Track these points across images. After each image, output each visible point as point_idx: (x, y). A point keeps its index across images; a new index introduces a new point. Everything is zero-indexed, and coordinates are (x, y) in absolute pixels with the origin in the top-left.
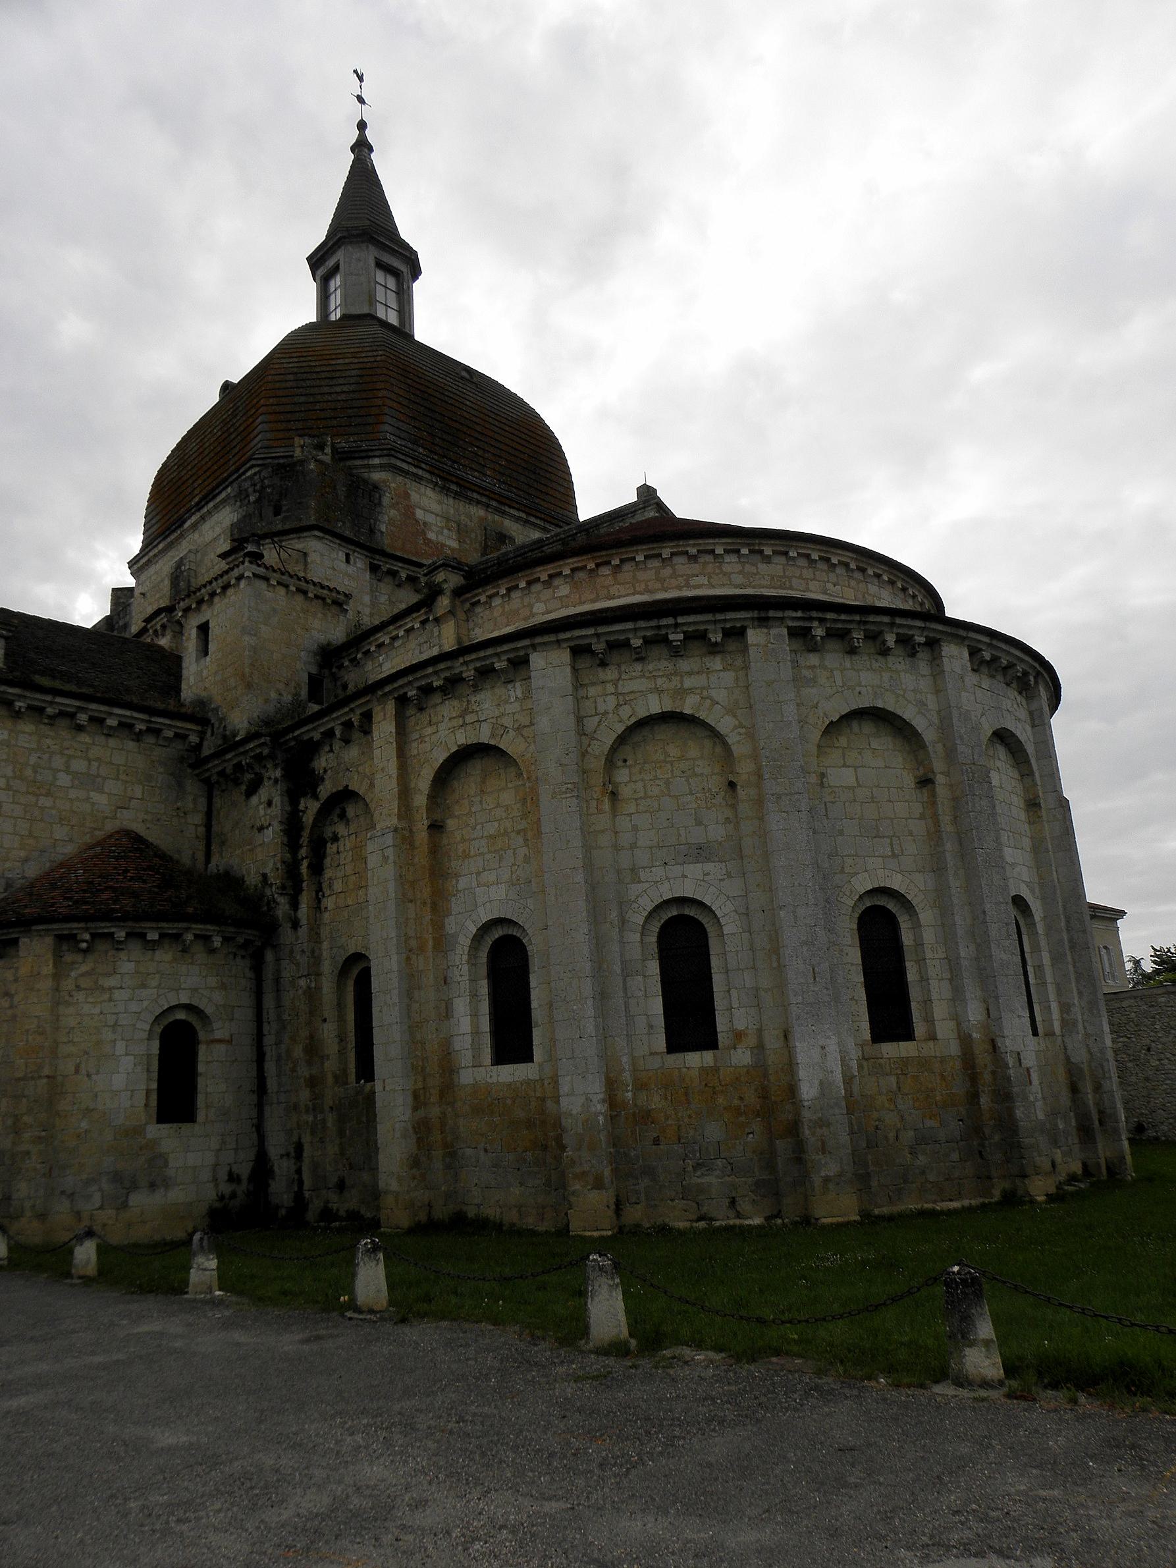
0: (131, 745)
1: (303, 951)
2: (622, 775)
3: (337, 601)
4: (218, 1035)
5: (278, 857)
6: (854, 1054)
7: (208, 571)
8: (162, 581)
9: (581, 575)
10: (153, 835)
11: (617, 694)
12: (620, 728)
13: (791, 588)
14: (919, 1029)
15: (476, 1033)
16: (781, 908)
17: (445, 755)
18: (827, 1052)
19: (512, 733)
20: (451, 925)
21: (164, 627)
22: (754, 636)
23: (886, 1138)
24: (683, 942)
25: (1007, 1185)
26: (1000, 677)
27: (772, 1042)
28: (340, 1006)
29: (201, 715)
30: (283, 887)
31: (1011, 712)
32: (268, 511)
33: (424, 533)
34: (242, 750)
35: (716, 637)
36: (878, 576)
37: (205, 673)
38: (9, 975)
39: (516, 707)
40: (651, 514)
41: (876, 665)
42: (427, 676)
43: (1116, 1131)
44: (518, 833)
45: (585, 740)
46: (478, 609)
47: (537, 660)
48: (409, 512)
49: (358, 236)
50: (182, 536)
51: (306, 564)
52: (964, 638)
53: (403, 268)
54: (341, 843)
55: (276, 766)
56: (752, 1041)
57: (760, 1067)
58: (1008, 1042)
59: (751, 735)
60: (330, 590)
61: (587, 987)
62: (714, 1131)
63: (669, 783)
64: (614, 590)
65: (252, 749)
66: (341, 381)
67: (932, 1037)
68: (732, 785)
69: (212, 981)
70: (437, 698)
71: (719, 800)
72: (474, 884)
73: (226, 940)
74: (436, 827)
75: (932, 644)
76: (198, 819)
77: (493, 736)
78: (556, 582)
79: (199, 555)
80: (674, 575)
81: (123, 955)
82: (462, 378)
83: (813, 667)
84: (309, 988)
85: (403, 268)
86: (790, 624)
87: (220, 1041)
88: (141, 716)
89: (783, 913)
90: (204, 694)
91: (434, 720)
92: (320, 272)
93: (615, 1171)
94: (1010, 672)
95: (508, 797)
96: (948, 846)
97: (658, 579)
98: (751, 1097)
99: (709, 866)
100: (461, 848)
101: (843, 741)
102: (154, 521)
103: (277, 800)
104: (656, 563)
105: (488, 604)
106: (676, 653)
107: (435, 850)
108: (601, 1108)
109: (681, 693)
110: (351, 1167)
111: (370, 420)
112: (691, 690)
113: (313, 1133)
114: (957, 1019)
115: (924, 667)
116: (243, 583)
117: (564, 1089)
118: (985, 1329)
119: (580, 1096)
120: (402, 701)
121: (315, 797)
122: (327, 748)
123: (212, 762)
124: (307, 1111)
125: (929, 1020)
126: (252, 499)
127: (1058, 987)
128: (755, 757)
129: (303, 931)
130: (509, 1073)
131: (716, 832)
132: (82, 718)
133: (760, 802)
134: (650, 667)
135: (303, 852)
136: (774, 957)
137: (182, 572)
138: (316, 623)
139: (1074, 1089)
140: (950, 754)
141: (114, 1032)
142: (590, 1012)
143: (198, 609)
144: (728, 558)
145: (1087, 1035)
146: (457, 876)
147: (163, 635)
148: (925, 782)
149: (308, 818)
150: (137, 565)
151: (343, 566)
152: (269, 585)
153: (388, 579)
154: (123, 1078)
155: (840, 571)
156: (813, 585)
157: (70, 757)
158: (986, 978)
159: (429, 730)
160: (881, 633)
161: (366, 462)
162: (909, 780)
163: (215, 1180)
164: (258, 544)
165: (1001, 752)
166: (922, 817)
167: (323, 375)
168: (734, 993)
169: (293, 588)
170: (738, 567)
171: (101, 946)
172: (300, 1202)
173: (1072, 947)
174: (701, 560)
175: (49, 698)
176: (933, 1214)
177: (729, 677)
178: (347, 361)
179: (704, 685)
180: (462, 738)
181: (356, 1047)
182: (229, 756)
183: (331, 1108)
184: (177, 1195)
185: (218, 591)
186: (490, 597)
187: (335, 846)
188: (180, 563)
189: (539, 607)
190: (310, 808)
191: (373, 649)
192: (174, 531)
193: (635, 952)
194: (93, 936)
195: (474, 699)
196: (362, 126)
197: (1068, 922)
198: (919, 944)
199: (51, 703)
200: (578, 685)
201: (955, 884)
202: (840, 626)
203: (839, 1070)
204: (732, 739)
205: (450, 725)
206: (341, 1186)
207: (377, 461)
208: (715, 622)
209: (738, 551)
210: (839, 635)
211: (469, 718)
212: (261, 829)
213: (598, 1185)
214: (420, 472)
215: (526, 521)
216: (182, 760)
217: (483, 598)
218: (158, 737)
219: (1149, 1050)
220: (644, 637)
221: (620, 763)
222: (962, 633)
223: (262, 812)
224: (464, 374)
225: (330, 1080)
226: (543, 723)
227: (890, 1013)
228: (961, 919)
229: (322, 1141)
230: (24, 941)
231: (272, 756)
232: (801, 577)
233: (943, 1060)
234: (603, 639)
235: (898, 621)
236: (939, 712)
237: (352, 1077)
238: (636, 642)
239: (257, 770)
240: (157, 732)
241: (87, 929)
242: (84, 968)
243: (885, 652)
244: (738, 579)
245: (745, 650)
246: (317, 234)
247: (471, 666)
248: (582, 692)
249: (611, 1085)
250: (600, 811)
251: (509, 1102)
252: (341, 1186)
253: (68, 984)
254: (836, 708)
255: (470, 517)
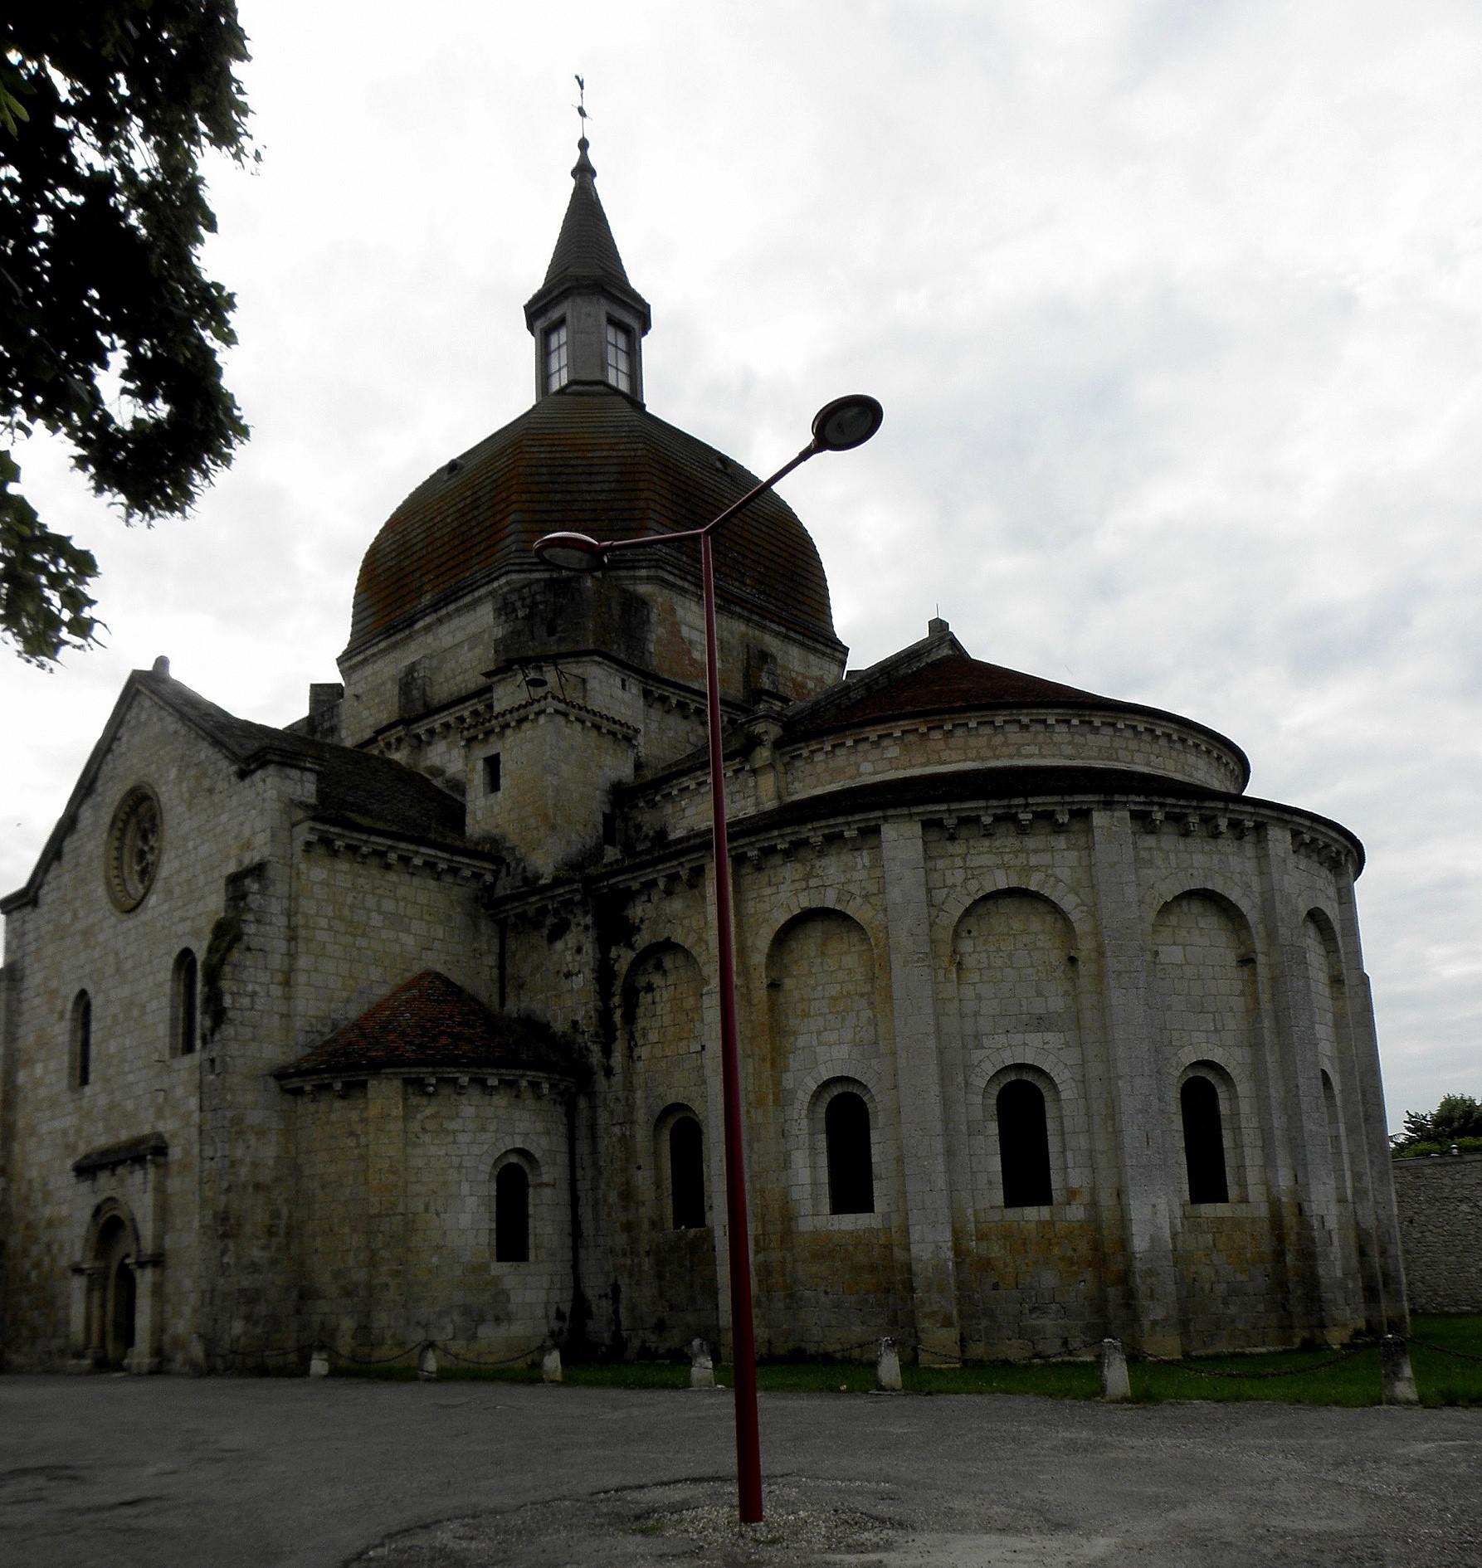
0: (433, 884)
1: (617, 1099)
2: (966, 946)
3: (624, 736)
4: (546, 1178)
5: (591, 1005)
6: (1179, 1212)
7: (447, 680)
8: (384, 684)
9: (911, 738)
10: (457, 977)
11: (966, 868)
12: (968, 902)
13: (1117, 760)
14: (1233, 1192)
15: (815, 1183)
16: (1120, 1077)
17: (787, 917)
18: (1156, 1211)
19: (859, 900)
20: (789, 1081)
21: (399, 740)
22: (1099, 819)
23: (1202, 1289)
24: (1021, 1105)
25: (1306, 1334)
26: (1315, 857)
27: (1106, 1199)
28: (656, 1154)
29: (493, 851)
30: (597, 1035)
31: (1320, 892)
32: (541, 631)
33: (689, 652)
34: (549, 894)
35: (1063, 818)
36: (1197, 746)
37: (496, 809)
38: (354, 1115)
39: (863, 875)
40: (945, 651)
41: (1207, 848)
42: (772, 838)
43: (1399, 1292)
44: (862, 995)
45: (934, 912)
46: (798, 763)
47: (889, 831)
48: (675, 631)
49: (587, 287)
50: (410, 637)
51: (585, 690)
52: (1288, 822)
53: (635, 324)
54: (657, 994)
55: (586, 913)
56: (1086, 1198)
57: (1094, 1221)
58: (1314, 1207)
59: (1093, 911)
60: (622, 725)
61: (938, 1145)
62: (1049, 1279)
63: (1016, 954)
64: (945, 755)
65: (561, 895)
66: (601, 478)
67: (1244, 1200)
68: (1072, 960)
69: (540, 1127)
70: (777, 860)
71: (1058, 974)
72: (815, 1043)
73: (552, 1086)
74: (774, 986)
75: (1260, 827)
76: (491, 960)
77: (839, 901)
78: (885, 743)
79: (435, 662)
80: (1006, 744)
81: (464, 1099)
82: (717, 470)
83: (1150, 849)
84: (624, 1135)
85: (635, 324)
86: (1133, 807)
87: (547, 1185)
88: (444, 855)
89: (1120, 1083)
90: (495, 831)
91: (773, 880)
92: (540, 324)
93: (960, 1311)
94: (1324, 852)
95: (850, 961)
96: (1266, 1023)
97: (989, 746)
98: (1084, 1248)
99: (1049, 1036)
100: (800, 1006)
101: (1173, 920)
102: (366, 614)
103: (588, 947)
104: (987, 730)
105: (810, 760)
106: (1023, 830)
107: (773, 1007)
108: (950, 1254)
109: (1027, 870)
110: (672, 1308)
111: (634, 525)
112: (1037, 868)
113: (631, 1276)
114: (1268, 1185)
115: (1249, 849)
116: (542, 719)
117: (915, 1236)
118: (1408, 1372)
119: (930, 1244)
120: (740, 860)
121: (631, 947)
122: (645, 898)
123: (509, 904)
124: (624, 1255)
125: (1242, 1184)
126: (520, 614)
127: (1352, 1156)
128: (1096, 933)
129: (617, 1079)
130: (848, 1222)
131: (1056, 1003)
132: (392, 857)
133: (1100, 976)
134: (998, 843)
135: (616, 1000)
136: (1110, 1123)
137: (414, 679)
138: (608, 760)
139: (1362, 1252)
140: (1272, 935)
141: (459, 1173)
142: (941, 1167)
143: (485, 740)
144: (1058, 729)
145: (1377, 1202)
146: (795, 1033)
147: (397, 749)
148: (1247, 961)
149: (622, 967)
150: (346, 661)
151: (619, 692)
152: (568, 721)
153: (657, 705)
154: (469, 1219)
155: (1163, 742)
156: (1138, 757)
157: (381, 897)
158: (1296, 1147)
159: (769, 891)
160: (1215, 817)
161: (631, 573)
162: (1231, 958)
163: (547, 1317)
164: (539, 669)
165: (1311, 930)
166: (1242, 994)
167: (580, 470)
168: (1069, 1154)
169: (589, 724)
170: (1068, 738)
171: (446, 1091)
172: (619, 1343)
173: (1367, 1120)
174: (1032, 729)
175: (364, 837)
176: (1243, 1355)
177: (1072, 856)
178: (605, 454)
179: (1051, 864)
180: (805, 901)
181: (673, 1194)
182: (533, 899)
183: (648, 1253)
184: (517, 1329)
185: (513, 724)
186: (812, 752)
187: (649, 997)
188: (412, 668)
189: (866, 767)
190: (623, 958)
191: (675, 792)
192: (401, 630)
193: (978, 1114)
194: (438, 1080)
195: (818, 864)
196: (583, 145)
197: (1364, 1095)
198: (1235, 1114)
199: (366, 842)
200: (928, 857)
201: (1271, 1059)
202: (1177, 810)
203: (1167, 1226)
204: (1074, 916)
205: (792, 887)
206: (661, 1327)
207: (643, 573)
208: (1063, 804)
209: (1068, 722)
210: (1176, 818)
211: (813, 882)
212: (568, 975)
213: (947, 1323)
214: (686, 585)
215: (786, 637)
216: (476, 899)
217: (805, 753)
218: (455, 876)
219: (1411, 1222)
220: (995, 815)
221: (964, 934)
222: (1287, 817)
223: (569, 958)
224: (718, 465)
225: (646, 1226)
226: (895, 894)
227: (1207, 1177)
228: (1275, 1092)
229: (638, 1283)
230: (372, 1084)
231: (583, 903)
232: (1126, 749)
233: (1254, 1221)
234: (954, 815)
235: (1231, 806)
236: (1262, 894)
237: (670, 1223)
238: (987, 820)
239: (563, 914)
240: (454, 871)
241: (433, 1074)
242: (429, 1111)
243: (1216, 835)
244: (1068, 750)
245: (1089, 830)
246: (534, 278)
247: (820, 833)
248: (931, 864)
249: (957, 1235)
250: (947, 980)
251: (851, 1248)
252: (661, 1327)
253: (415, 1126)
254: (1170, 889)
255: (732, 633)
